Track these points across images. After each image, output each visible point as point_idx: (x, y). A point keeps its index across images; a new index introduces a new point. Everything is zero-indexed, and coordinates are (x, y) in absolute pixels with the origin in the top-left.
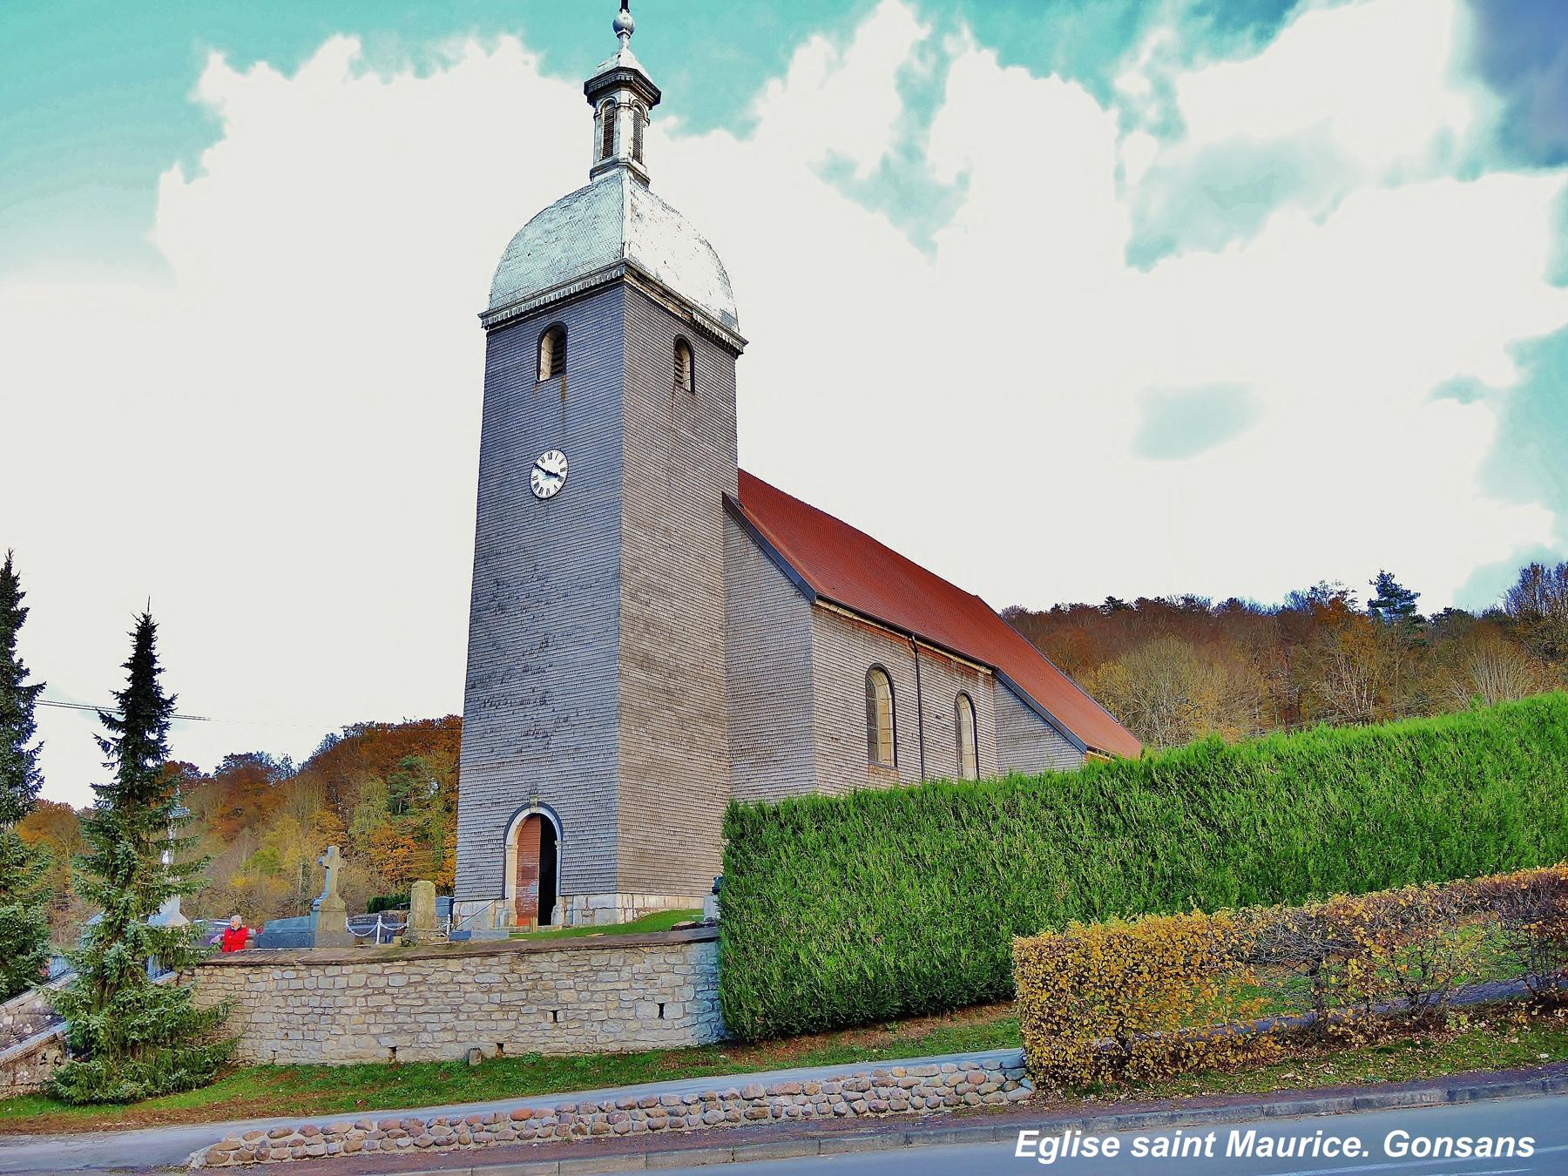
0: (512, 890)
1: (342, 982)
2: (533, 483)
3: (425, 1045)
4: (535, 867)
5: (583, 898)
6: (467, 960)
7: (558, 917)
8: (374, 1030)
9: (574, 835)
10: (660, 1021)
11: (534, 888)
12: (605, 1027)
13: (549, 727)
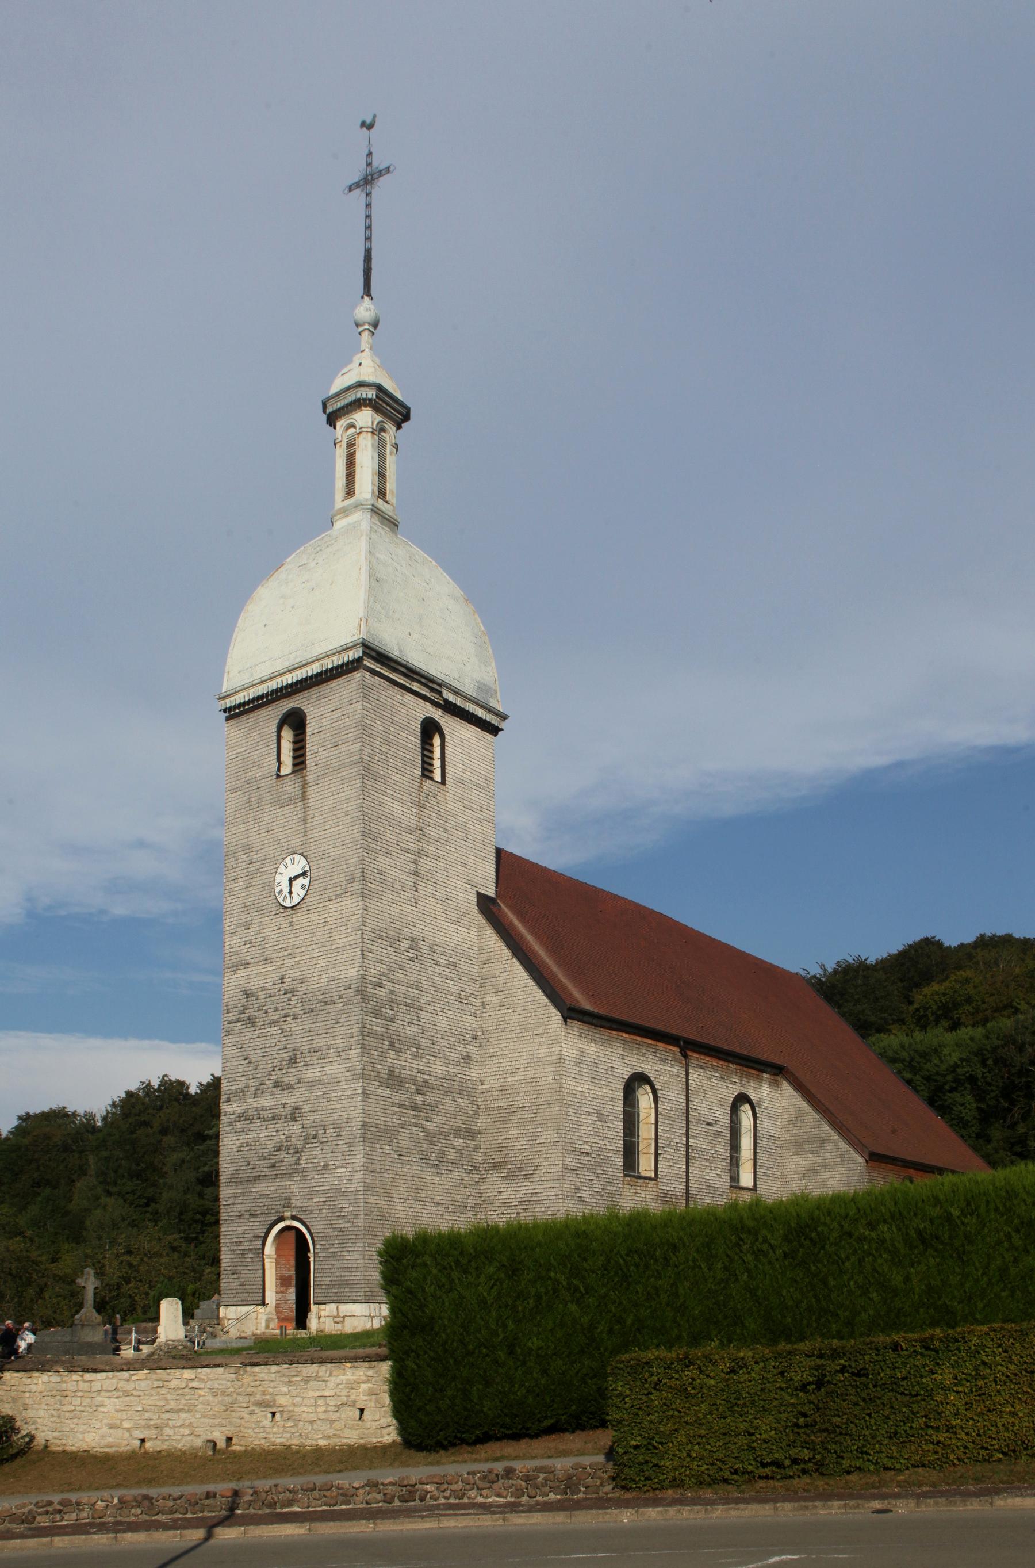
0: (271, 1297)
1: (97, 1386)
2: (277, 889)
3: (167, 1438)
4: (290, 1276)
5: (333, 1306)
6: (200, 1370)
7: (313, 1323)
8: (126, 1425)
9: (324, 1249)
10: (360, 1422)
11: (291, 1295)
12: (315, 1426)
13: (299, 1144)
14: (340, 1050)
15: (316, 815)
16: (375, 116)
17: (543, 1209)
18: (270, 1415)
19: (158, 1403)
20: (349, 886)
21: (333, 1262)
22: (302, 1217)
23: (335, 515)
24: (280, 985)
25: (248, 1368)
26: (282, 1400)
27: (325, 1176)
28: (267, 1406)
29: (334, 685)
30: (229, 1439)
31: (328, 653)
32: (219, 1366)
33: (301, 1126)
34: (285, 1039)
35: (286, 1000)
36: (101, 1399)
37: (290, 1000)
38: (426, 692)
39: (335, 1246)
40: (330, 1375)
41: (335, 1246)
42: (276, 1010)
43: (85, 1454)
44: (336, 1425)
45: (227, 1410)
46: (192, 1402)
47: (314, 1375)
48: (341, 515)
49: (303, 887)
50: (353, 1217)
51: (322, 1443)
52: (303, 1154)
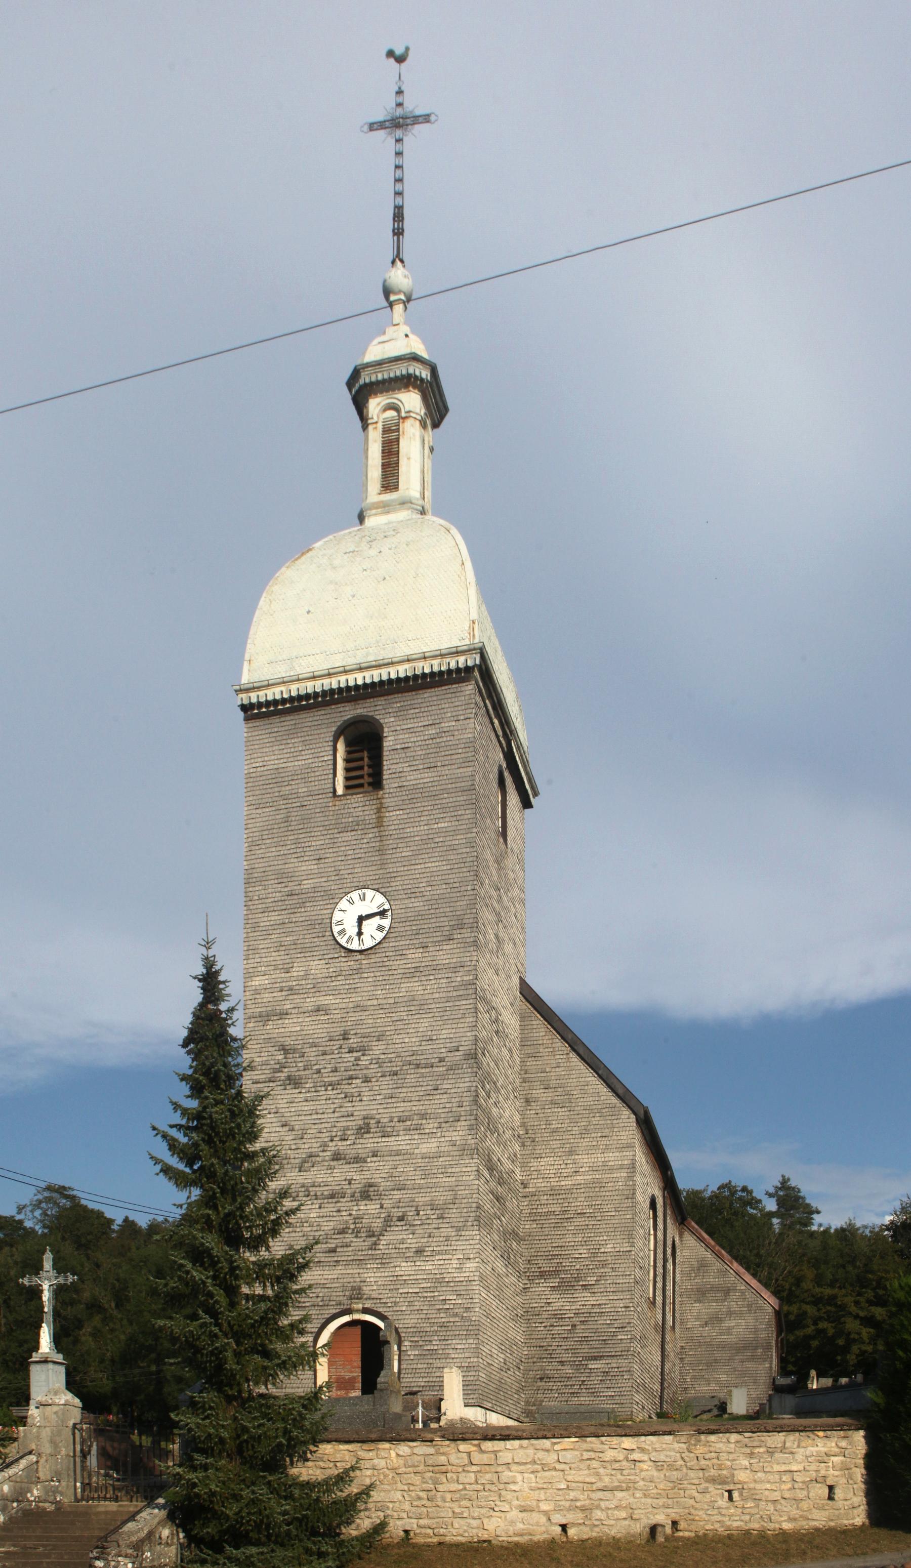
6: (643, 1438)
8: (544, 1507)
9: (415, 1344)
13: (377, 1224)
14: (442, 1120)
15: (400, 845)
16: (407, 49)
17: (608, 1322)
18: (726, 1494)
19: (587, 1480)
20: (455, 932)
21: (431, 1361)
22: (380, 1310)
23: (370, 509)
24: (341, 1042)
25: (703, 1437)
26: (742, 1476)
27: (418, 1263)
28: (724, 1482)
29: (425, 695)
30: (675, 1523)
31: (427, 655)
32: (665, 1433)
33: (378, 1206)
34: (350, 1104)
35: (353, 1059)
36: (511, 1474)
37: (358, 1059)
38: (500, 733)
39: (434, 1343)
40: (798, 1446)
41: (434, 1343)
42: (335, 1070)
43: (485, 1545)
44: (805, 1505)
45: (675, 1487)
46: (632, 1477)
47: (780, 1445)
48: (379, 510)
49: (380, 928)
50: (462, 1310)
51: (786, 1526)
52: (381, 1238)
